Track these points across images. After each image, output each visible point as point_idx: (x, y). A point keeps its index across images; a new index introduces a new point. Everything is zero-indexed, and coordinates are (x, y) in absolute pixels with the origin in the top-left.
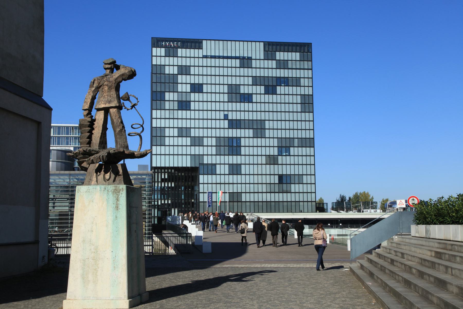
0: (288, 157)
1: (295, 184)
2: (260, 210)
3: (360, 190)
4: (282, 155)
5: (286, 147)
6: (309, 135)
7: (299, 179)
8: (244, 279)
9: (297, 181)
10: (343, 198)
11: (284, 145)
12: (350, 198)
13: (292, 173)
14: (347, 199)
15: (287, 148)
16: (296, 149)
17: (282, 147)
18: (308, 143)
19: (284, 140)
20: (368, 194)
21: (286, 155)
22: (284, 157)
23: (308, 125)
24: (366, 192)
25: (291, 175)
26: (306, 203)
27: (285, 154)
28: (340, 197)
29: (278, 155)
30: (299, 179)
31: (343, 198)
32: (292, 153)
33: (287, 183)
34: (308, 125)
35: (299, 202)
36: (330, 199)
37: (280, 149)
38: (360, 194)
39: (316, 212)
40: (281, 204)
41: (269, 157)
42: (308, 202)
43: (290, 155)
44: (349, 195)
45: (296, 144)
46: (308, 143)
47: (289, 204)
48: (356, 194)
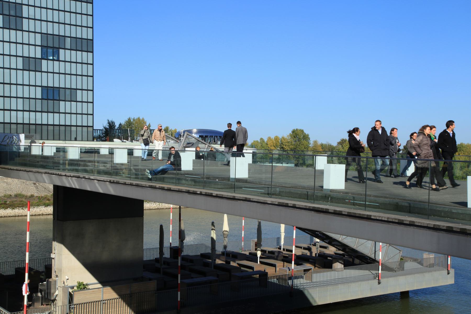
0: (56, 63)
1: (65, 101)
2: (62, 136)
3: (134, 115)
4: (48, 60)
5: (53, 48)
6: (85, 34)
7: (71, 94)
8: (451, 135)
9: (68, 98)
10: (111, 125)
11: (50, 44)
12: (120, 124)
13: (62, 86)
14: (117, 126)
15: (56, 50)
16: (68, 52)
17: (47, 47)
18: (85, 45)
19: (50, 37)
20: (308, 135)
21: (53, 60)
22: (50, 63)
23: (85, 21)
24: (141, 118)
25: (59, 88)
26: (80, 129)
27: (51, 58)
28: (109, 123)
29: (42, 59)
30: (71, 94)
31: (111, 125)
32: (62, 58)
33: (54, 100)
34: (85, 21)
35: (71, 126)
36: (100, 124)
37: (45, 49)
38: (134, 120)
39: (93, 141)
40: (45, 128)
41: (26, 59)
42: (82, 126)
43: (58, 60)
44: (119, 120)
45: (68, 46)
46: (85, 45)
47: (57, 128)
48: (129, 119)
